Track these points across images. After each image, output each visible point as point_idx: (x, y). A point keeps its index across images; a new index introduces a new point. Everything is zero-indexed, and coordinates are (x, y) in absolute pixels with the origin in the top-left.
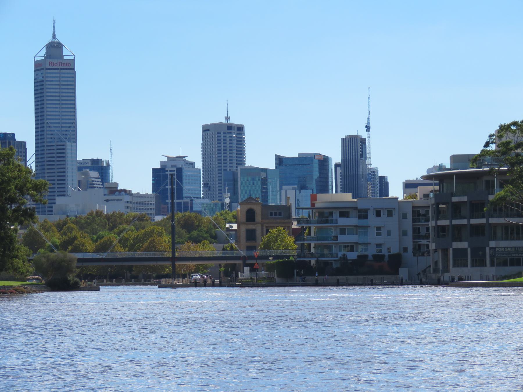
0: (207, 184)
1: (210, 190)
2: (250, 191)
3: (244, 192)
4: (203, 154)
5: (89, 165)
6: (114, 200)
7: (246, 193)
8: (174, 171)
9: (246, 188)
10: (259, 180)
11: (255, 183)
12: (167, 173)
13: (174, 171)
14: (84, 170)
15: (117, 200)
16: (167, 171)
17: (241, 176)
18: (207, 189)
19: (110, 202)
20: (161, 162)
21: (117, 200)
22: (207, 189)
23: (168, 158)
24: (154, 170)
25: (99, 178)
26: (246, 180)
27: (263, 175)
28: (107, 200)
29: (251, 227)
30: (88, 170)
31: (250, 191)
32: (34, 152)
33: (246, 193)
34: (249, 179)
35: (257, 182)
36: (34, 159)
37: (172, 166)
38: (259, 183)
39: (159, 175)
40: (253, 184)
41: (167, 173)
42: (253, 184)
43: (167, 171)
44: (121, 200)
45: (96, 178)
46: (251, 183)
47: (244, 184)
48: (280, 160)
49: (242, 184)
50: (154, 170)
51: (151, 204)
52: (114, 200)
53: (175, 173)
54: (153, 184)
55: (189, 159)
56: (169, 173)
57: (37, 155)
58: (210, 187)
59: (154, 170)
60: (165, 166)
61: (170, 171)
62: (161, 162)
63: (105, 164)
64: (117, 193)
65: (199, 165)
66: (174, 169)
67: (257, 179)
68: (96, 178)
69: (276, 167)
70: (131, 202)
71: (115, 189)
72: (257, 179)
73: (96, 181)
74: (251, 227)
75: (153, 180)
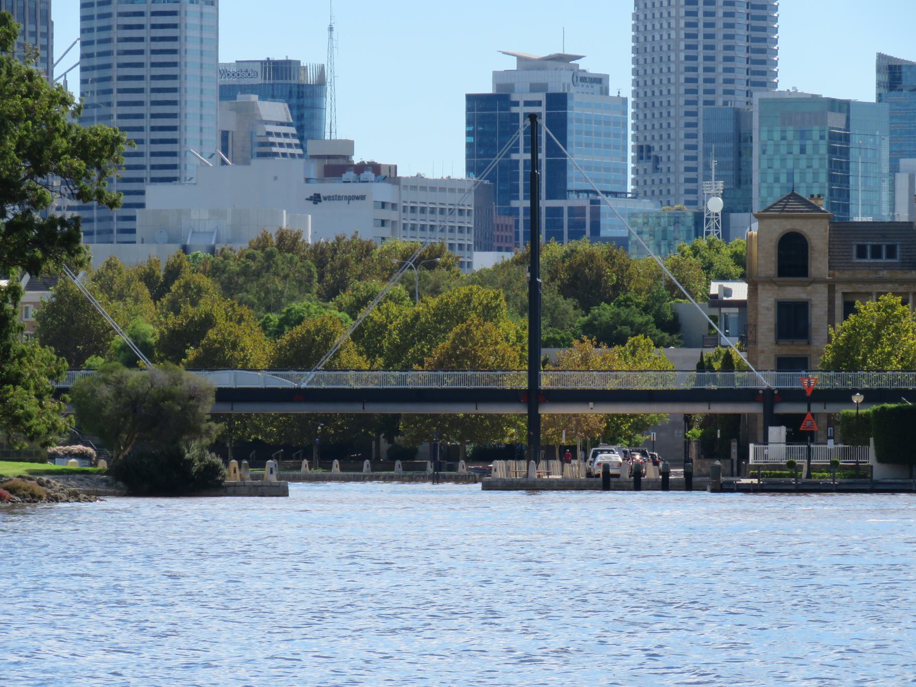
0: (649, 149)
1: (656, 169)
2: (791, 176)
3: (770, 179)
4: (636, 50)
5: (259, 80)
6: (339, 198)
7: (777, 180)
8: (539, 103)
9: (777, 164)
10: (822, 138)
11: (809, 149)
12: (514, 110)
13: (539, 103)
14: (241, 98)
15: (350, 198)
16: (516, 104)
18: (649, 165)
20: (496, 75)
21: (350, 198)
22: (649, 165)
23: (521, 59)
24: (473, 101)
25: (289, 125)
26: (777, 136)
27: (836, 121)
28: (316, 199)
30: (254, 98)
31: (791, 176)
32: (78, 34)
33: (777, 180)
34: (790, 135)
35: (816, 145)
36: (75, 55)
37: (534, 88)
38: (823, 150)
39: (489, 117)
40: (803, 151)
41: (514, 110)
42: (803, 151)
43: (516, 104)
44: (363, 198)
46: (796, 150)
47: (770, 150)
49: (764, 152)
50: (470, 98)
52: (339, 198)
53: (542, 110)
54: (469, 145)
55: (590, 66)
56: (521, 110)
58: (657, 159)
59: (470, 98)
60: (511, 87)
61: (528, 104)
62: (496, 75)
63: (311, 78)
65: (622, 84)
66: (541, 97)
67: (816, 135)
68: (282, 124)
69: (880, 97)
70: (394, 206)
71: (341, 162)
72: (816, 135)
73: (278, 135)
74: (793, 293)
75: (469, 134)
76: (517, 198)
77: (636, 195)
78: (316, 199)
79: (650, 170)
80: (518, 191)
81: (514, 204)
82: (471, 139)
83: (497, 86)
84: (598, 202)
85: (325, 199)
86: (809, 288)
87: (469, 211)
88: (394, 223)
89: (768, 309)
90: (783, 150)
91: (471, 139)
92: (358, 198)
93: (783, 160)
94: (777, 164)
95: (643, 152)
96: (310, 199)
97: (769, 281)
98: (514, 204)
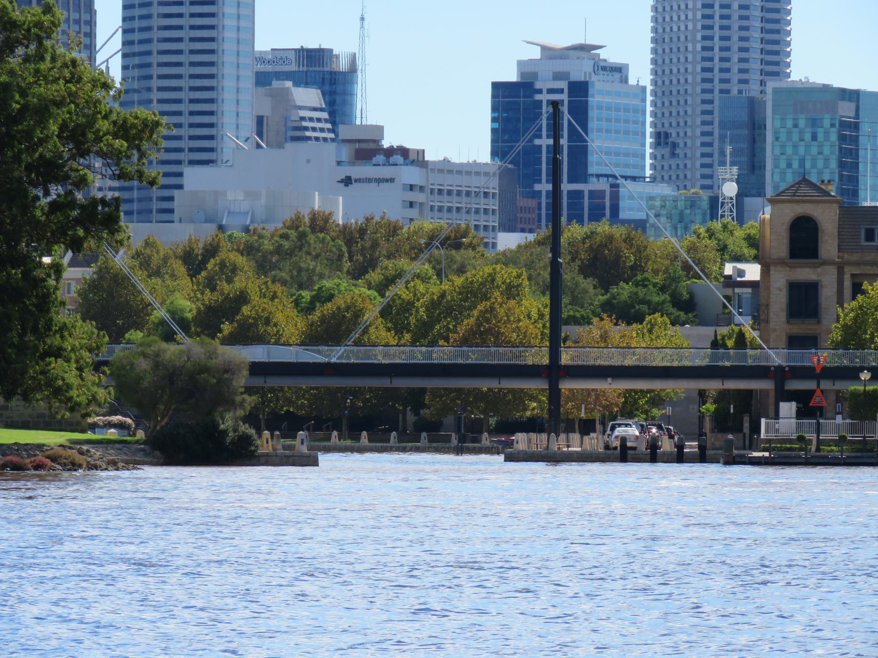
0: (667, 135)
1: (673, 155)
2: (802, 161)
3: (783, 165)
4: (654, 40)
5: (293, 67)
6: (369, 180)
7: (789, 165)
8: (561, 91)
9: (789, 151)
10: (833, 125)
11: (820, 137)
12: (538, 97)
13: (561, 91)
14: (276, 84)
15: (379, 181)
16: (540, 91)
17: (774, 113)
18: (666, 151)
19: (355, 185)
20: (520, 63)
22: (666, 151)
23: (544, 48)
24: (499, 88)
26: (789, 123)
28: (347, 181)
29: (805, 274)
30: (289, 84)
31: (802, 161)
32: (120, 24)
33: (789, 165)
34: (802, 123)
35: (827, 133)
36: (117, 43)
37: (557, 76)
38: (834, 137)
39: (514, 104)
40: (814, 138)
41: (538, 97)
42: (814, 138)
43: (540, 91)
44: (392, 180)
45: (315, 109)
46: (808, 136)
47: (783, 137)
48: (315, 463)
49: (777, 139)
50: (496, 86)
51: (486, 194)
52: (369, 180)
53: (564, 97)
54: (494, 131)
55: (610, 55)
56: (544, 97)
57: (125, 32)
58: (674, 145)
59: (496, 86)
60: (535, 75)
61: (551, 91)
62: (520, 63)
63: (343, 65)
64: (380, 158)
65: (641, 73)
66: (563, 85)
67: (827, 123)
68: (315, 109)
70: (422, 189)
71: (372, 146)
72: (827, 123)
73: (311, 119)
74: (805, 274)
75: (494, 120)
76: (540, 181)
77: (654, 179)
78: (347, 181)
79: (667, 155)
80: (540, 175)
81: (537, 187)
82: (496, 125)
83: (522, 74)
84: (617, 186)
85: (356, 181)
86: (819, 270)
87: (494, 194)
88: (421, 204)
89: (780, 290)
90: (796, 137)
91: (496, 125)
92: (387, 181)
93: (795, 147)
94: (789, 151)
95: (661, 138)
96: (342, 181)
97: (781, 262)
98: (537, 187)
